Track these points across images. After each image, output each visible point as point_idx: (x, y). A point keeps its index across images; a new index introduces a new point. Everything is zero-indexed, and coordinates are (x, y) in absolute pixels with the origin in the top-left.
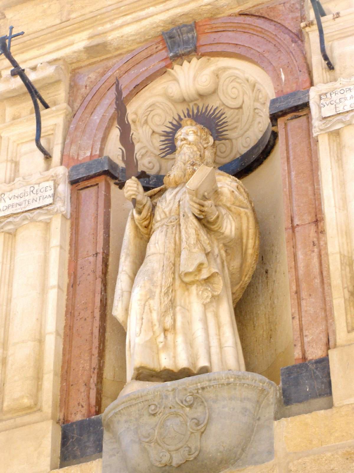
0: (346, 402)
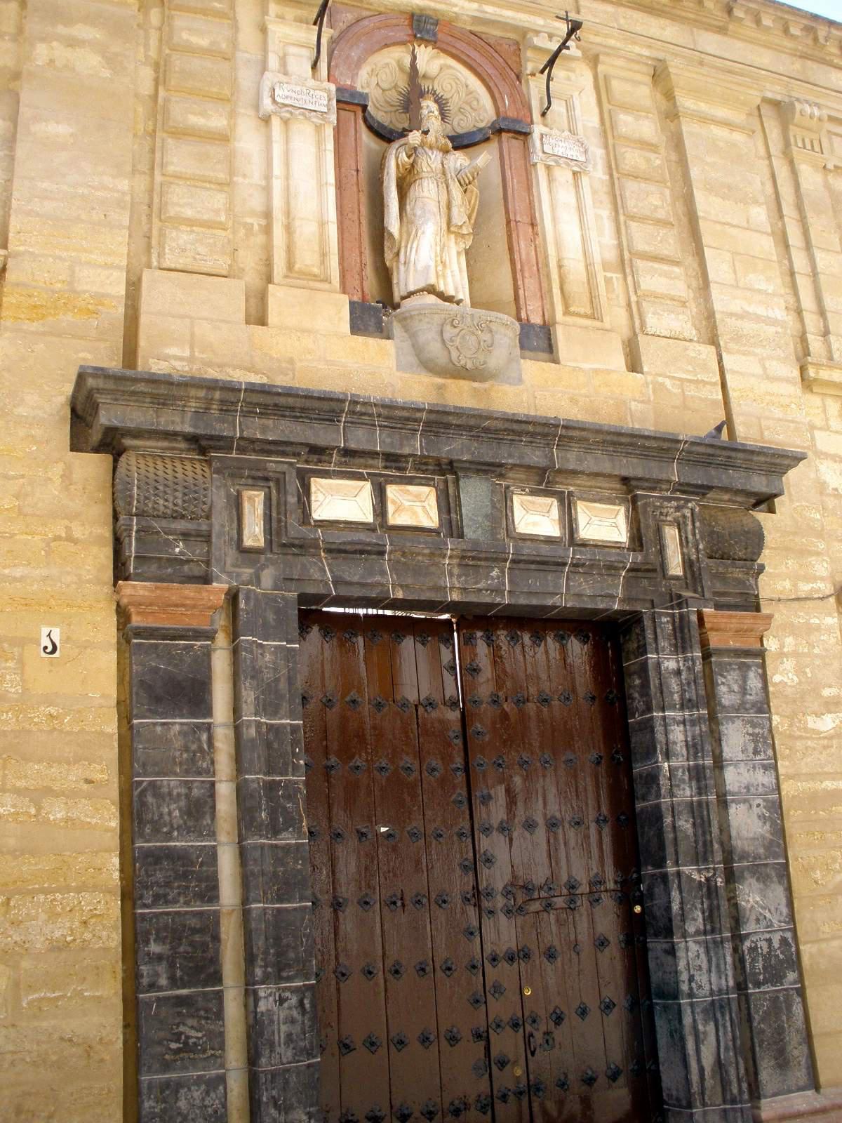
0: (569, 364)
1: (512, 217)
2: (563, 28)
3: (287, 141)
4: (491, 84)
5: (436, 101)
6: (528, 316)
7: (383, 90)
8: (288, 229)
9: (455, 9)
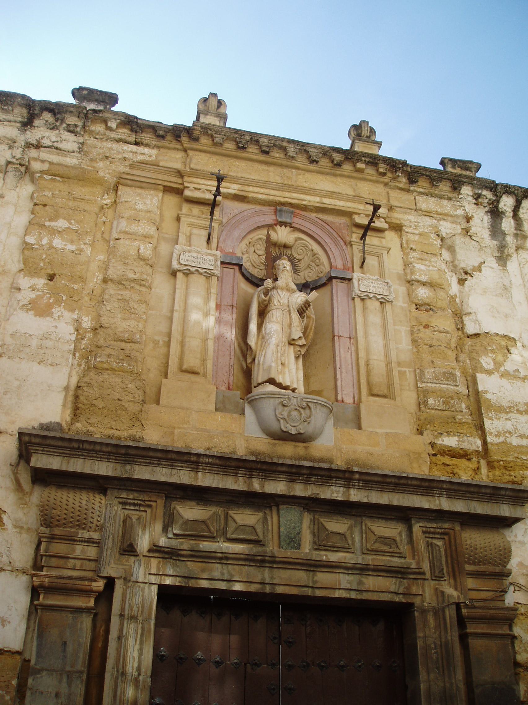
0: (368, 429)
1: (336, 333)
2: (371, 208)
3: (187, 287)
4: (327, 249)
5: (290, 260)
6: (342, 398)
7: (259, 256)
8: (182, 344)
9: (304, 203)
